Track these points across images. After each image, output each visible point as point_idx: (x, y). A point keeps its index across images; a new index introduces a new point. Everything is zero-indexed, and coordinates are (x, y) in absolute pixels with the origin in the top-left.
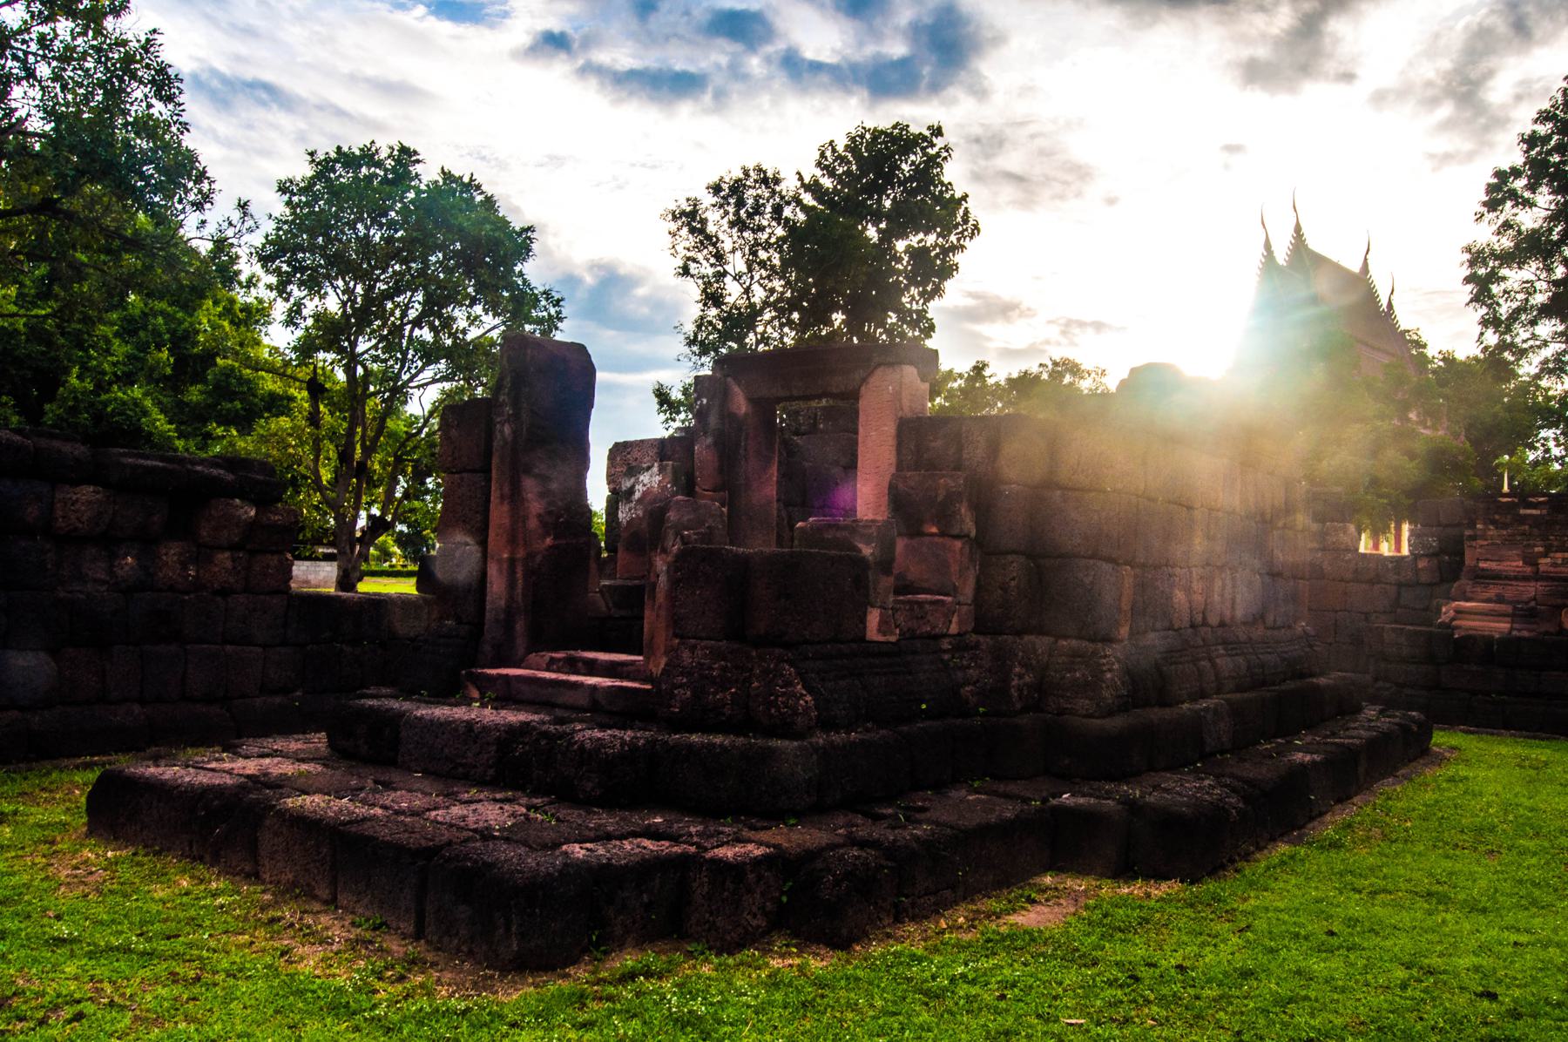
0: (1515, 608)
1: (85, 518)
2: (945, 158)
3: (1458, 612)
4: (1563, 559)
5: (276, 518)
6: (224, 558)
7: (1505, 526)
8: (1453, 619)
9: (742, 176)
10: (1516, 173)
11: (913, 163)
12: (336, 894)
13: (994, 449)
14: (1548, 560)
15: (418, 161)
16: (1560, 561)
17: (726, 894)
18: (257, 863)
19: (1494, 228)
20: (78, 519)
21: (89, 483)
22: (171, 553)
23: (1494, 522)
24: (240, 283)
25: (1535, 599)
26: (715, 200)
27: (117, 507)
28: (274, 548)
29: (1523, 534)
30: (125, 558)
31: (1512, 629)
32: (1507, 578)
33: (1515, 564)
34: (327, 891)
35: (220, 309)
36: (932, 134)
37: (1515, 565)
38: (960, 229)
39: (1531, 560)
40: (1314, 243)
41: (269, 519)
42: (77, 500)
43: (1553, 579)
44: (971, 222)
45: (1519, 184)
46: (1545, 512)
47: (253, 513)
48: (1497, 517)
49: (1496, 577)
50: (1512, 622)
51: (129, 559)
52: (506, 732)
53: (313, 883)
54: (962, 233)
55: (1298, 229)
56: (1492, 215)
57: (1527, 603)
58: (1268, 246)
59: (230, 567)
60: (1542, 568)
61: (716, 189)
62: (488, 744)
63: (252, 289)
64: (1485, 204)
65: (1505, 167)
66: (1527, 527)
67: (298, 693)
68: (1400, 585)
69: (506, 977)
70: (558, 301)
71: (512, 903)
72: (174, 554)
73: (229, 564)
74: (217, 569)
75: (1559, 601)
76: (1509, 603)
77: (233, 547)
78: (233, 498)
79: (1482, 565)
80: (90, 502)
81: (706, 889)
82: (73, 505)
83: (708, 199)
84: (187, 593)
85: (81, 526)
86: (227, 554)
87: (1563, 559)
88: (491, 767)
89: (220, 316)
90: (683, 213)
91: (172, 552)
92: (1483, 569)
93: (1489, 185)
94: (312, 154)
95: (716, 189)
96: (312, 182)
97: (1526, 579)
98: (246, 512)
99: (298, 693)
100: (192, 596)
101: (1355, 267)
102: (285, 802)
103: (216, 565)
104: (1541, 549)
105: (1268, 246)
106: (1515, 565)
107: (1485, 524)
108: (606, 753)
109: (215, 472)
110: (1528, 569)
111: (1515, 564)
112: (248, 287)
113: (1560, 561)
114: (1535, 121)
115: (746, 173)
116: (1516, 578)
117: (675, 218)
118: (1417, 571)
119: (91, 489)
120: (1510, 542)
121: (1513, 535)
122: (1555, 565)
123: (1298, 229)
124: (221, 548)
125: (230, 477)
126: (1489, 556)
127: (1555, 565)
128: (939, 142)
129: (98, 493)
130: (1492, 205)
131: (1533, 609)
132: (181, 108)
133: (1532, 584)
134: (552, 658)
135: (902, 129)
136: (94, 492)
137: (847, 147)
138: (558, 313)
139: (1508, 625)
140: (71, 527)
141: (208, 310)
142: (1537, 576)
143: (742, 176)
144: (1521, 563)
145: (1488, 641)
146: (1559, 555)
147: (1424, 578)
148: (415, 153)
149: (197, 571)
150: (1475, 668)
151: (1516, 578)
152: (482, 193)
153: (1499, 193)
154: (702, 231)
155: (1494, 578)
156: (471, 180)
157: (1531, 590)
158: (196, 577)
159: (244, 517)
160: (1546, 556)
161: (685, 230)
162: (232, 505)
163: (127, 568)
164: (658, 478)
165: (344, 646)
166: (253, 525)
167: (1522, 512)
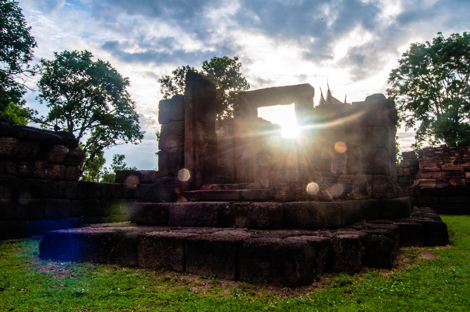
0: (437, 180)
1: (9, 149)
2: (240, 66)
3: (420, 182)
4: (448, 165)
5: (76, 153)
6: (57, 167)
7: (431, 157)
8: (419, 184)
9: (183, 69)
10: (397, 70)
11: (230, 68)
12: (185, 268)
13: (27, 240)
14: (444, 166)
15: (92, 56)
16: (447, 166)
17: (352, 251)
18: (137, 260)
19: (393, 85)
20: (7, 150)
21: (11, 136)
22: (39, 164)
23: (428, 156)
24: (19, 103)
25: (442, 177)
26: (175, 76)
27: (21, 146)
28: (74, 164)
29: (437, 159)
30: (23, 166)
31: (436, 186)
32: (433, 171)
33: (435, 167)
34: (180, 267)
35: (13, 110)
36: (235, 60)
37: (435, 168)
38: (244, 87)
39: (439, 166)
40: (333, 95)
41: (73, 153)
42: (7, 142)
43: (447, 171)
44: (248, 85)
45: (398, 73)
46: (442, 152)
47: (68, 151)
48: (429, 154)
49: (430, 171)
50: (436, 184)
51: (25, 166)
52: (220, 206)
53: (172, 265)
54: (245, 88)
55: (329, 91)
56: (392, 82)
57: (439, 178)
58: (322, 95)
59: (59, 171)
60: (443, 168)
61: (175, 73)
62: (213, 211)
63: (23, 105)
64: (389, 79)
65: (395, 68)
66: (437, 157)
67: (82, 217)
68: (399, 177)
69: (295, 289)
70: (133, 102)
71: (296, 256)
72: (40, 165)
73: (59, 170)
74: (55, 171)
75: (449, 177)
76: (435, 178)
77: (60, 163)
78: (61, 145)
79: (425, 168)
80: (11, 144)
81: (342, 251)
82: (5, 144)
83: (172, 76)
84: (44, 179)
85: (7, 152)
86: (58, 166)
87: (448, 165)
88: (215, 220)
89: (14, 112)
90: (165, 81)
91: (40, 164)
92: (426, 169)
93: (390, 74)
94: (56, 53)
95: (175, 73)
96: (56, 62)
97: (438, 171)
98: (66, 151)
99: (82, 217)
100: (46, 181)
101: (343, 102)
102: (280, 194)
103: (54, 170)
104: (442, 163)
105: (322, 95)
106: (435, 168)
107: (425, 156)
108: (271, 208)
109: (56, 135)
110: (439, 169)
111: (435, 167)
112: (22, 104)
113: (447, 166)
114: (402, 56)
115: (184, 68)
116: (436, 171)
117: (162, 82)
118: (404, 172)
119: (12, 139)
120: (433, 161)
121: (434, 159)
122: (446, 167)
123: (329, 91)
124: (56, 164)
125: (61, 137)
126: (427, 166)
127: (446, 167)
128: (237, 62)
129: (14, 140)
130: (392, 79)
131: (441, 180)
132: (25, 24)
133: (441, 173)
134: (213, 186)
135: (226, 58)
136: (13, 140)
137: (210, 63)
138: (133, 106)
139: (435, 185)
140: (4, 153)
141: (9, 110)
142: (441, 171)
143: (183, 69)
144: (436, 167)
145: (431, 189)
146: (447, 164)
147: (406, 174)
148: (91, 53)
149: (48, 171)
150: (428, 197)
151: (436, 171)
152: (111, 67)
153: (393, 76)
154: (170, 85)
155: (429, 172)
156: (108, 63)
157: (440, 175)
158: (48, 174)
159: (65, 152)
160: (443, 164)
161: (165, 86)
162: (61, 147)
163: (24, 169)
164: (223, 132)
165: (97, 200)
166: (68, 155)
167: (436, 152)
